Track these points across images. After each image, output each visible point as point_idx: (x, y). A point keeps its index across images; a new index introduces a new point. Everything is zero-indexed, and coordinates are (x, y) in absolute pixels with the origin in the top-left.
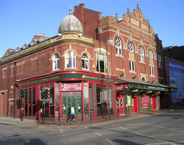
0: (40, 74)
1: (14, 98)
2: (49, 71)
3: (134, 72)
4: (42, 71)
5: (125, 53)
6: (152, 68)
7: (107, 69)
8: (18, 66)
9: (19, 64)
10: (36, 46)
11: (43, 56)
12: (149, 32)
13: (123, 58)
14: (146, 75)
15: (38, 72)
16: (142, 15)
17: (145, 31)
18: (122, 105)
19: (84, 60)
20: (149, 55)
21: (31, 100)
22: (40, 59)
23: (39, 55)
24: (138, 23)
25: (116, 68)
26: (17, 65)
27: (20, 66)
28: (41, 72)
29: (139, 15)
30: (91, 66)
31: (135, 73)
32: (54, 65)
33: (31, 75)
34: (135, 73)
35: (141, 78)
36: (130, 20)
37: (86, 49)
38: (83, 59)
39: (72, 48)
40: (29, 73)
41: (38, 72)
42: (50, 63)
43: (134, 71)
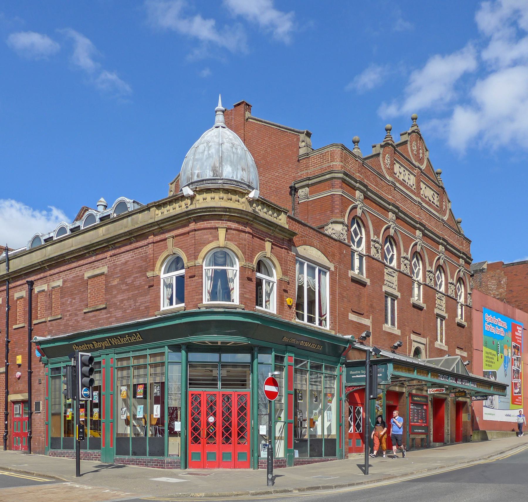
0: (117, 320)
4: (124, 311)
9: (45, 287)
10: (102, 231)
11: (126, 262)
14: (423, 340)
15: (109, 315)
21: (114, 341)
22: (117, 273)
25: (350, 314)
26: (36, 290)
27: (49, 294)
28: (119, 314)
29: (418, 151)
32: (164, 293)
35: (413, 349)
36: (392, 164)
39: (226, 239)
40: (76, 315)
41: (109, 315)
42: (153, 284)
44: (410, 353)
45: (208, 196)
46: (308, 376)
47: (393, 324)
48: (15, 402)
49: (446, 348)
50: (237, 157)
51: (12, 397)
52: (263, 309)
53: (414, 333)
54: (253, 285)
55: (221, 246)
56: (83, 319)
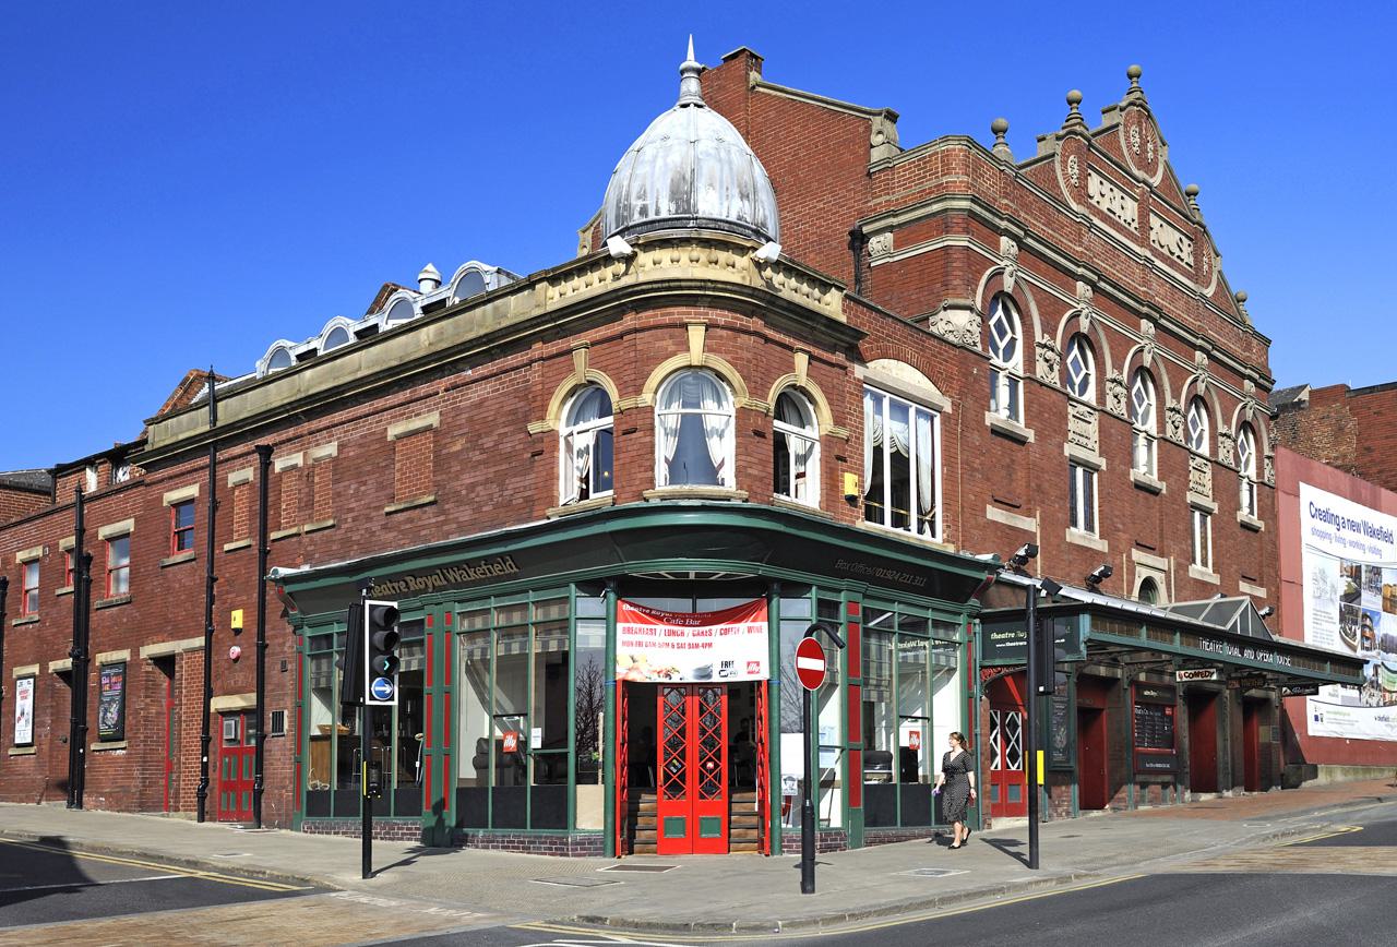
0: (461, 529)
1: (254, 696)
2: (529, 506)
3: (1097, 543)
4: (477, 510)
5: (1048, 405)
7: (927, 505)
8: (286, 470)
9: (297, 459)
12: (1197, 274)
13: (1032, 439)
14: (1162, 563)
15: (442, 518)
16: (1155, 151)
17: (1172, 264)
20: (1186, 430)
23: (454, 393)
25: (989, 507)
26: (279, 465)
27: (307, 474)
28: (465, 515)
29: (1143, 145)
31: (1102, 546)
33: (391, 535)
34: (1102, 546)
36: (1084, 177)
37: (801, 361)
39: (707, 348)
41: (442, 518)
42: (543, 449)
43: (1097, 536)
44: (1130, 591)
47: (1089, 527)
49: (1215, 580)
50: (731, 169)
51: (218, 703)
52: (886, 528)
54: (767, 448)
55: (695, 363)
56: (385, 527)
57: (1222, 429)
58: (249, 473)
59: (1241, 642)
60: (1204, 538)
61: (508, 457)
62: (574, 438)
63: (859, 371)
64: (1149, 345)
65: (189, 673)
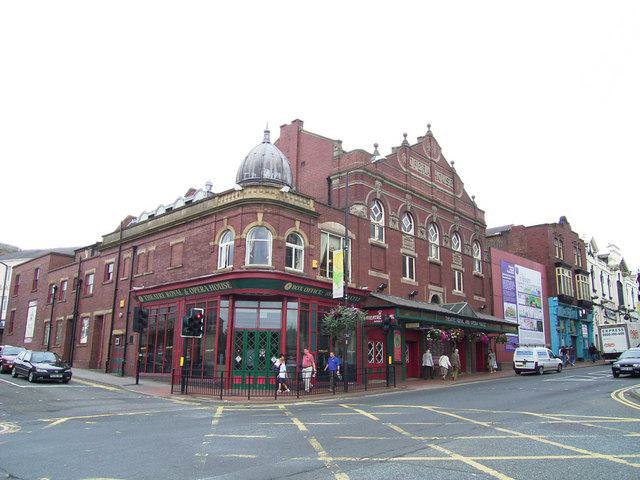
6: (459, 274)
9: (144, 251)
14: (441, 290)
18: (379, 358)
19: (290, 249)
24: (427, 169)
26: (139, 252)
27: (148, 255)
28: (190, 271)
30: (308, 263)
37: (298, 223)
38: (288, 244)
42: (215, 250)
45: (253, 190)
46: (73, 370)
47: (411, 277)
48: (117, 336)
51: (115, 332)
52: (293, 269)
53: (431, 283)
54: (284, 253)
57: (466, 242)
58: (130, 255)
59: (464, 318)
60: (459, 280)
61: (204, 253)
62: (225, 244)
63: (320, 226)
64: (378, 190)
65: (108, 322)
